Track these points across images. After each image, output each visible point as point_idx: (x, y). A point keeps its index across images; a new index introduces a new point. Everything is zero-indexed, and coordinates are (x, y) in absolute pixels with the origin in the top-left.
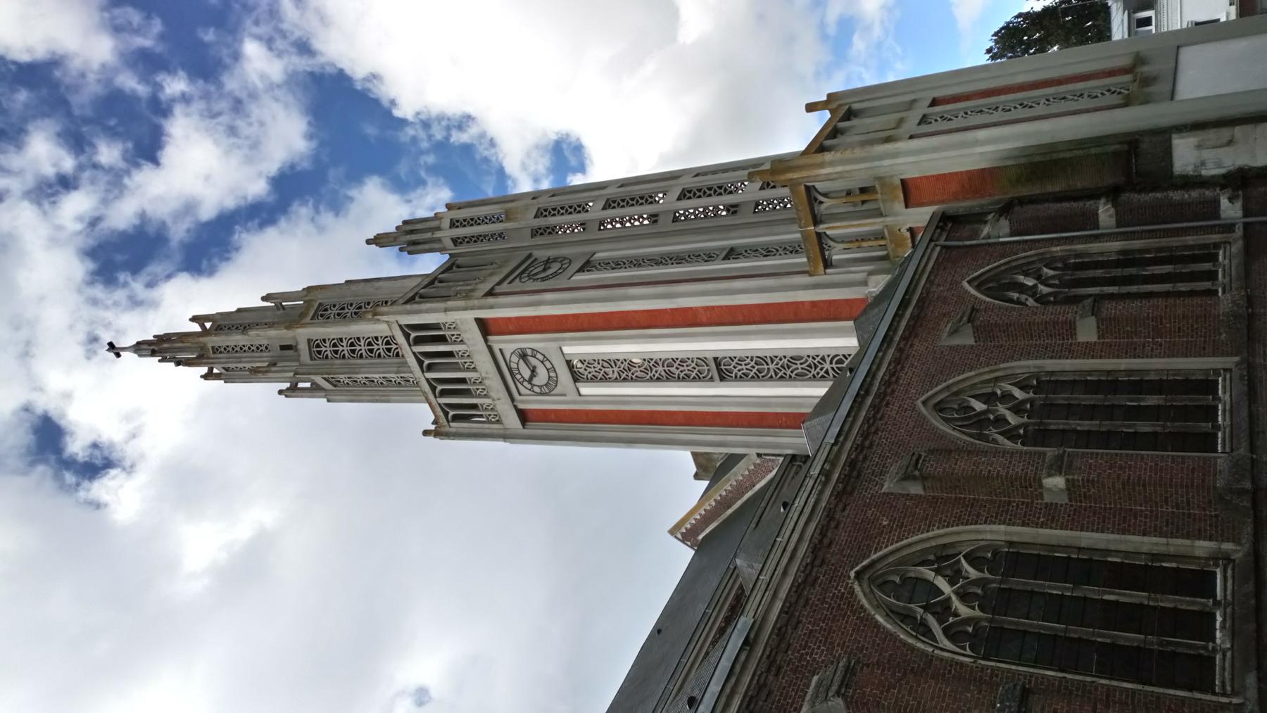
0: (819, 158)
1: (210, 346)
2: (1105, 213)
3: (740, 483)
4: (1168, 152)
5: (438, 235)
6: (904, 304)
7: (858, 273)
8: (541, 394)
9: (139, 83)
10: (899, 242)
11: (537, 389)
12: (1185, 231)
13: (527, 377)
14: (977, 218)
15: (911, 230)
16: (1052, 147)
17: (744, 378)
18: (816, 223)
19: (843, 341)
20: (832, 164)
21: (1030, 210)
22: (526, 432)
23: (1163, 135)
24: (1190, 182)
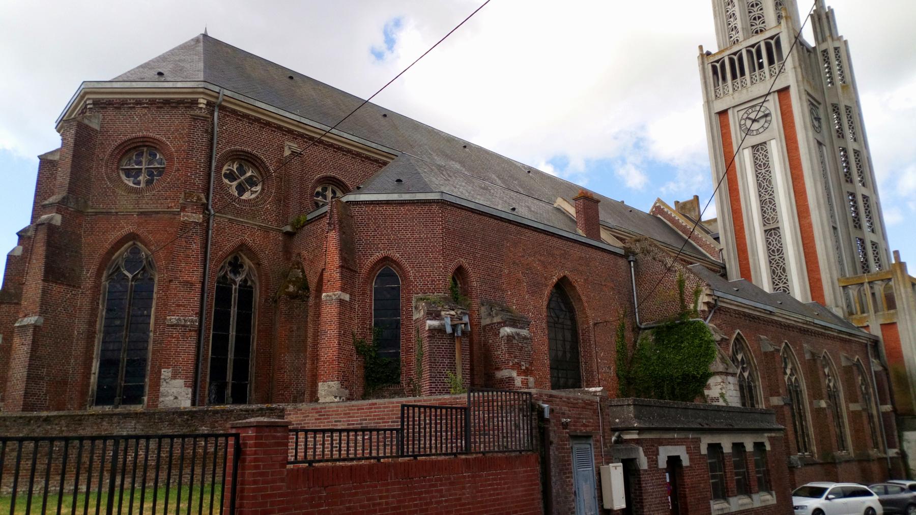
0: (909, 285)
2: (888, 408)
3: (701, 239)
5: (829, 40)
6: (850, 334)
7: (842, 302)
8: (740, 125)
11: (743, 122)
12: (882, 437)
13: (750, 116)
14: (877, 355)
15: (868, 326)
18: (869, 283)
19: (798, 290)
20: (906, 292)
21: (885, 378)
22: (713, 115)
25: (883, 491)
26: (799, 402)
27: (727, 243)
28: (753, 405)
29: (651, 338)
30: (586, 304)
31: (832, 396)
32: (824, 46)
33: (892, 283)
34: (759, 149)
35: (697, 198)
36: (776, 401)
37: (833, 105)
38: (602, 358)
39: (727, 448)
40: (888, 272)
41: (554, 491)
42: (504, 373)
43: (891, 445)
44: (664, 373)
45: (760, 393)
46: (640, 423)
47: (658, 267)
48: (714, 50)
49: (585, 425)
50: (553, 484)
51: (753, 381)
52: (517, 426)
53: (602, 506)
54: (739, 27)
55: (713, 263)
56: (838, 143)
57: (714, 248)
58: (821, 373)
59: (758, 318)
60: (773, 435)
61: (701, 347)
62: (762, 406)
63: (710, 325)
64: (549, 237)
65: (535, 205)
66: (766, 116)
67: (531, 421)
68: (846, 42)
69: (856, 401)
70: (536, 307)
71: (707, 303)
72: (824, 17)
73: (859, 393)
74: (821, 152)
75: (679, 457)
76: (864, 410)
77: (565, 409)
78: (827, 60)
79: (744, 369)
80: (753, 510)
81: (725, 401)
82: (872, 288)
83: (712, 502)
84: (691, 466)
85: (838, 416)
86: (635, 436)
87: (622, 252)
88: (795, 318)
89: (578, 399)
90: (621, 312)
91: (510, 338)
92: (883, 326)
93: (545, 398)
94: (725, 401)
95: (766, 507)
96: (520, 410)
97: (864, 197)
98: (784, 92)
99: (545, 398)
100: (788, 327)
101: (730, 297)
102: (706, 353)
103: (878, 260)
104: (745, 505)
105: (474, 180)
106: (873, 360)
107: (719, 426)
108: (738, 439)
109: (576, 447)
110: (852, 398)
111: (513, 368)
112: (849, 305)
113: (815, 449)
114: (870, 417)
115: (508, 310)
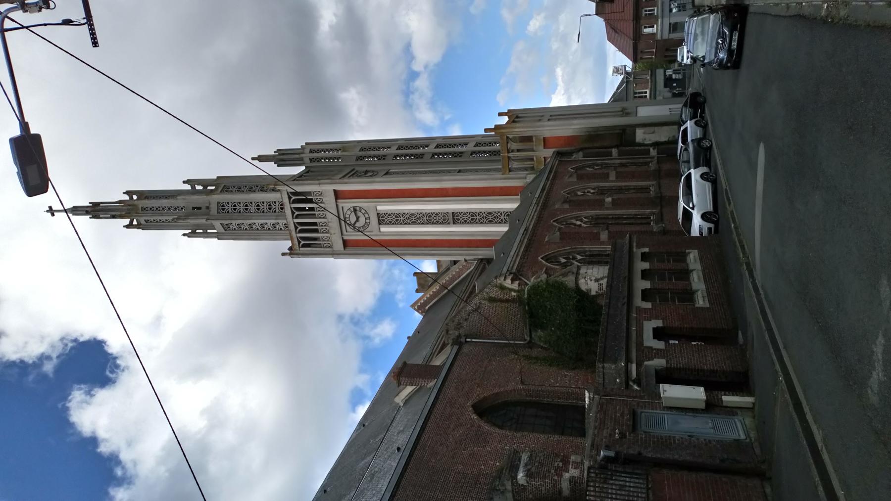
0: (514, 125)
1: (140, 206)
2: (614, 152)
3: (453, 276)
4: (635, 133)
6: (550, 172)
7: (523, 174)
9: (331, 27)
10: (539, 162)
14: (570, 154)
16: (597, 129)
17: (465, 222)
19: (510, 205)
23: (634, 127)
24: (640, 145)
25: (686, 164)
26: (606, 217)
27: (460, 255)
28: (608, 255)
29: (540, 333)
30: (502, 389)
31: (602, 191)
32: (307, 160)
33: (511, 136)
34: (383, 219)
35: (415, 274)
36: (604, 236)
37: (357, 160)
38: (557, 381)
39: (647, 285)
40: (502, 139)
41: (688, 458)
42: (565, 486)
43: (648, 152)
44: (576, 329)
45: (596, 248)
46: (621, 361)
47: (475, 317)
48: (289, 244)
49: (622, 415)
50: (681, 459)
51: (586, 251)
52: (622, 488)
53: (702, 410)
54: (273, 222)
55: (476, 268)
56: (389, 160)
57: (463, 266)
58: (582, 198)
59: (529, 240)
60: (635, 244)
61: (551, 292)
62: (609, 248)
63: (532, 281)
64: (432, 417)
65: (398, 425)
66: (355, 210)
67: (617, 472)
68: (307, 144)
69: (608, 174)
70: (500, 441)
71: (513, 281)
72: (282, 157)
73: (601, 171)
74: (394, 173)
75: (654, 329)
76: (615, 169)
77: (605, 433)
78: (319, 160)
79: (574, 258)
80: (703, 271)
81: (602, 279)
82: (513, 151)
83: (697, 305)
84: (663, 319)
85: (620, 190)
86: (634, 366)
87: (456, 348)
88: (532, 212)
89: (596, 417)
90: (513, 356)
91: (529, 474)
92: (545, 147)
93: (594, 453)
94: (602, 279)
95: (701, 259)
96: (605, 482)
97: (437, 147)
98: (338, 195)
99: (594, 453)
100: (540, 218)
101: (509, 260)
102: (559, 287)
103: (490, 144)
104: (699, 277)
105: (361, 487)
106: (574, 157)
107: (626, 288)
108: (638, 275)
109: (643, 428)
110: (606, 177)
111: (560, 476)
112: (526, 169)
113: (648, 211)
114: (622, 165)
115: (500, 471)
